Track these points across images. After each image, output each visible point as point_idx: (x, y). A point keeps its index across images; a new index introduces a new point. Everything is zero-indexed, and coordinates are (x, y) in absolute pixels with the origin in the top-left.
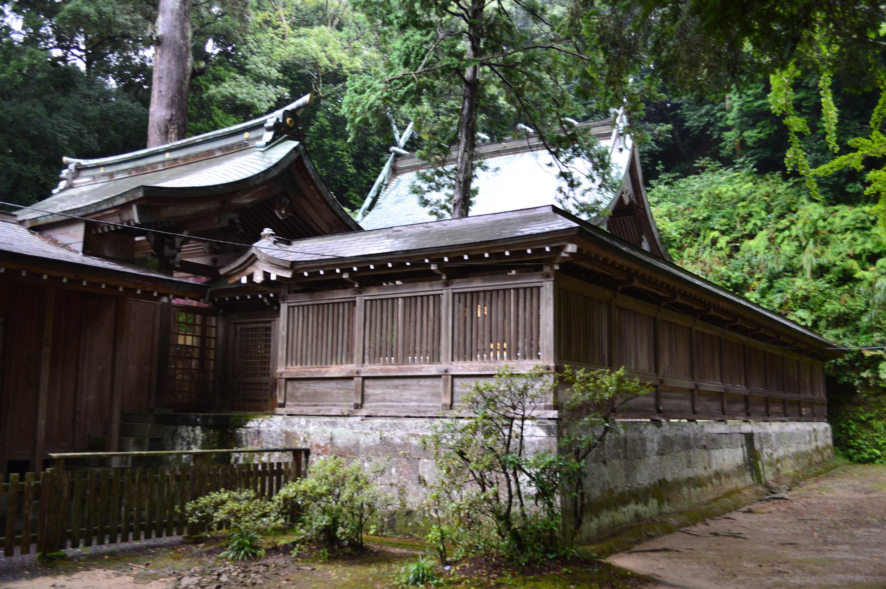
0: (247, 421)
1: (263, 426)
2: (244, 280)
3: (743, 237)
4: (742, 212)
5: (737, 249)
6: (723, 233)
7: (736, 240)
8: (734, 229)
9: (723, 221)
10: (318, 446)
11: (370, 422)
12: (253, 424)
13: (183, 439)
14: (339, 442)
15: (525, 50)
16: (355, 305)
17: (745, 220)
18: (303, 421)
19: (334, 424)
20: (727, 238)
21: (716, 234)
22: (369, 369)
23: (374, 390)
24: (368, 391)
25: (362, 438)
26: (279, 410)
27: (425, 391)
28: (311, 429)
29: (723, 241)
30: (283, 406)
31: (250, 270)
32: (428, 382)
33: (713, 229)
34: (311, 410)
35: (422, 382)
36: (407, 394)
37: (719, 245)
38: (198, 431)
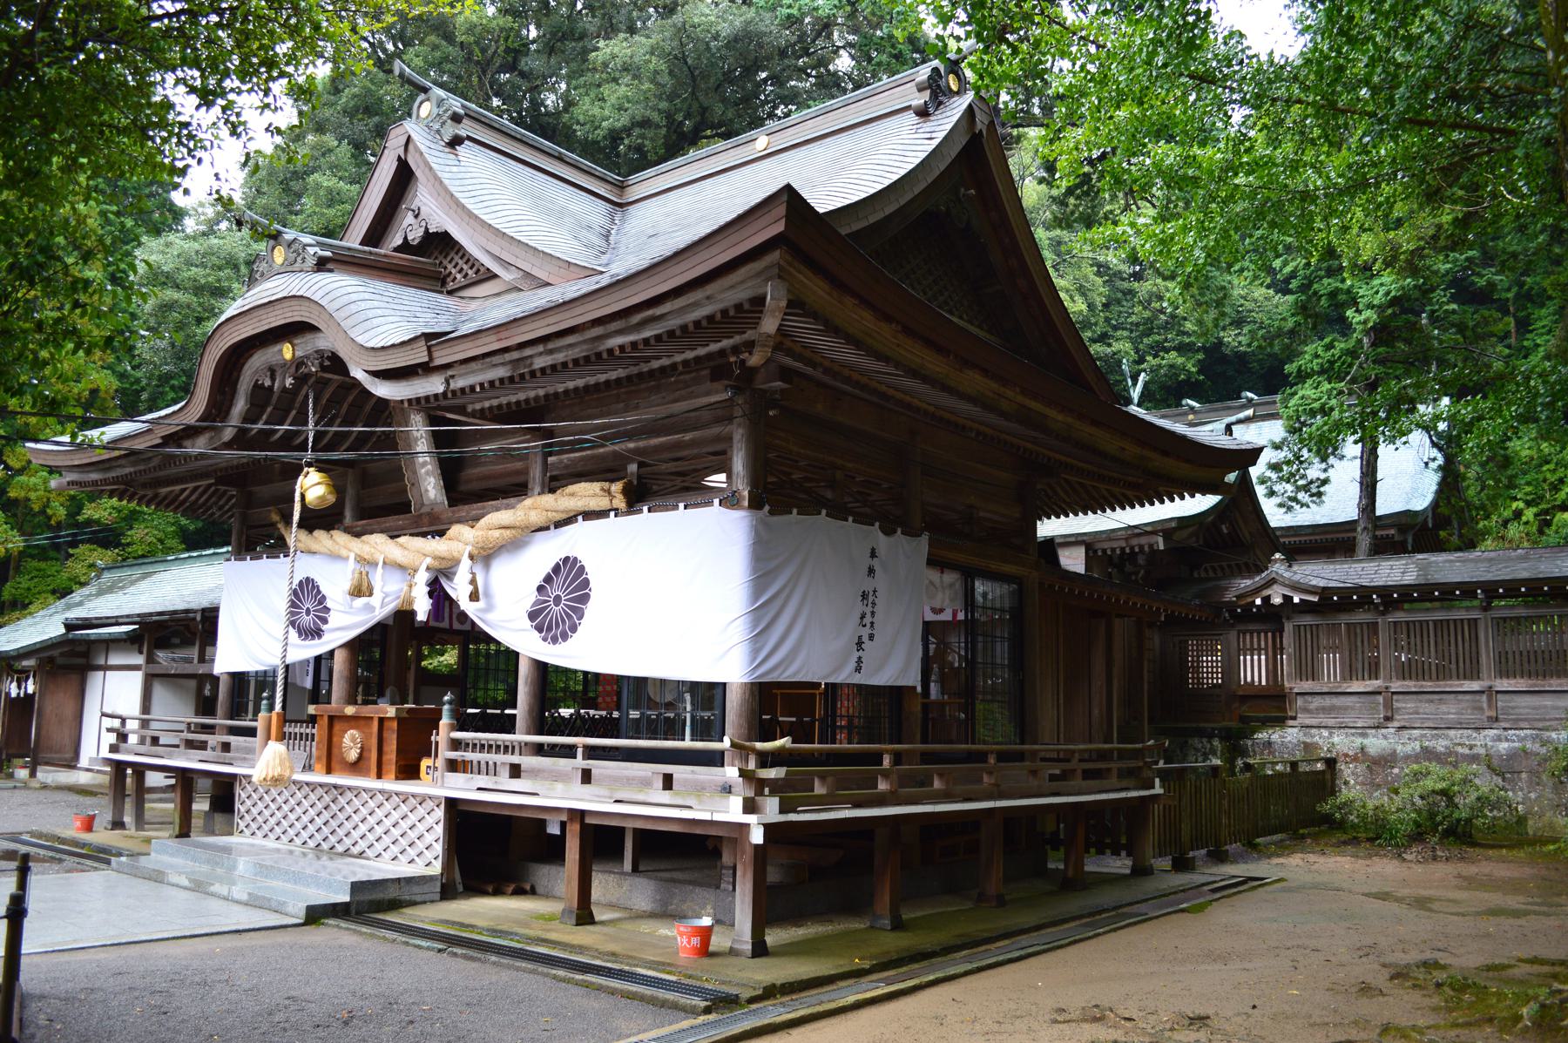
0: (1254, 733)
1: (1275, 737)
2: (1258, 602)
3: (1554, 507)
4: (1552, 478)
5: (1548, 524)
6: (1529, 504)
7: (1546, 512)
8: (1542, 498)
9: (1528, 489)
10: (1346, 755)
11: (1406, 733)
12: (1262, 736)
13: (1197, 750)
14: (1372, 751)
15: (1072, 96)
16: (1376, 633)
17: (1555, 488)
18: (1325, 733)
19: (1364, 735)
20: (1533, 510)
21: (1521, 505)
22: (1396, 686)
23: (1502, 702)
24: (1396, 705)
25: (1399, 748)
26: (1291, 722)
27: (1464, 705)
28: (1336, 739)
29: (1529, 514)
30: (1294, 718)
31: (1265, 593)
32: (1468, 697)
33: (1515, 499)
34: (1331, 722)
35: (1460, 697)
36: (1444, 708)
37: (1524, 519)
38: (1216, 743)
